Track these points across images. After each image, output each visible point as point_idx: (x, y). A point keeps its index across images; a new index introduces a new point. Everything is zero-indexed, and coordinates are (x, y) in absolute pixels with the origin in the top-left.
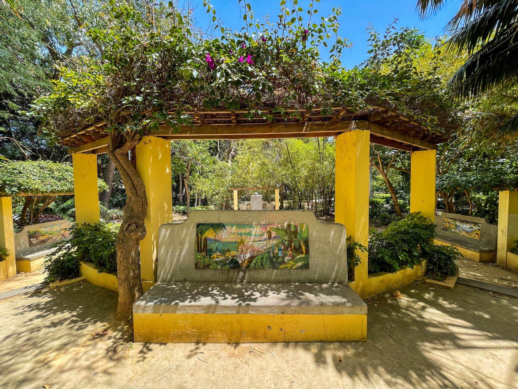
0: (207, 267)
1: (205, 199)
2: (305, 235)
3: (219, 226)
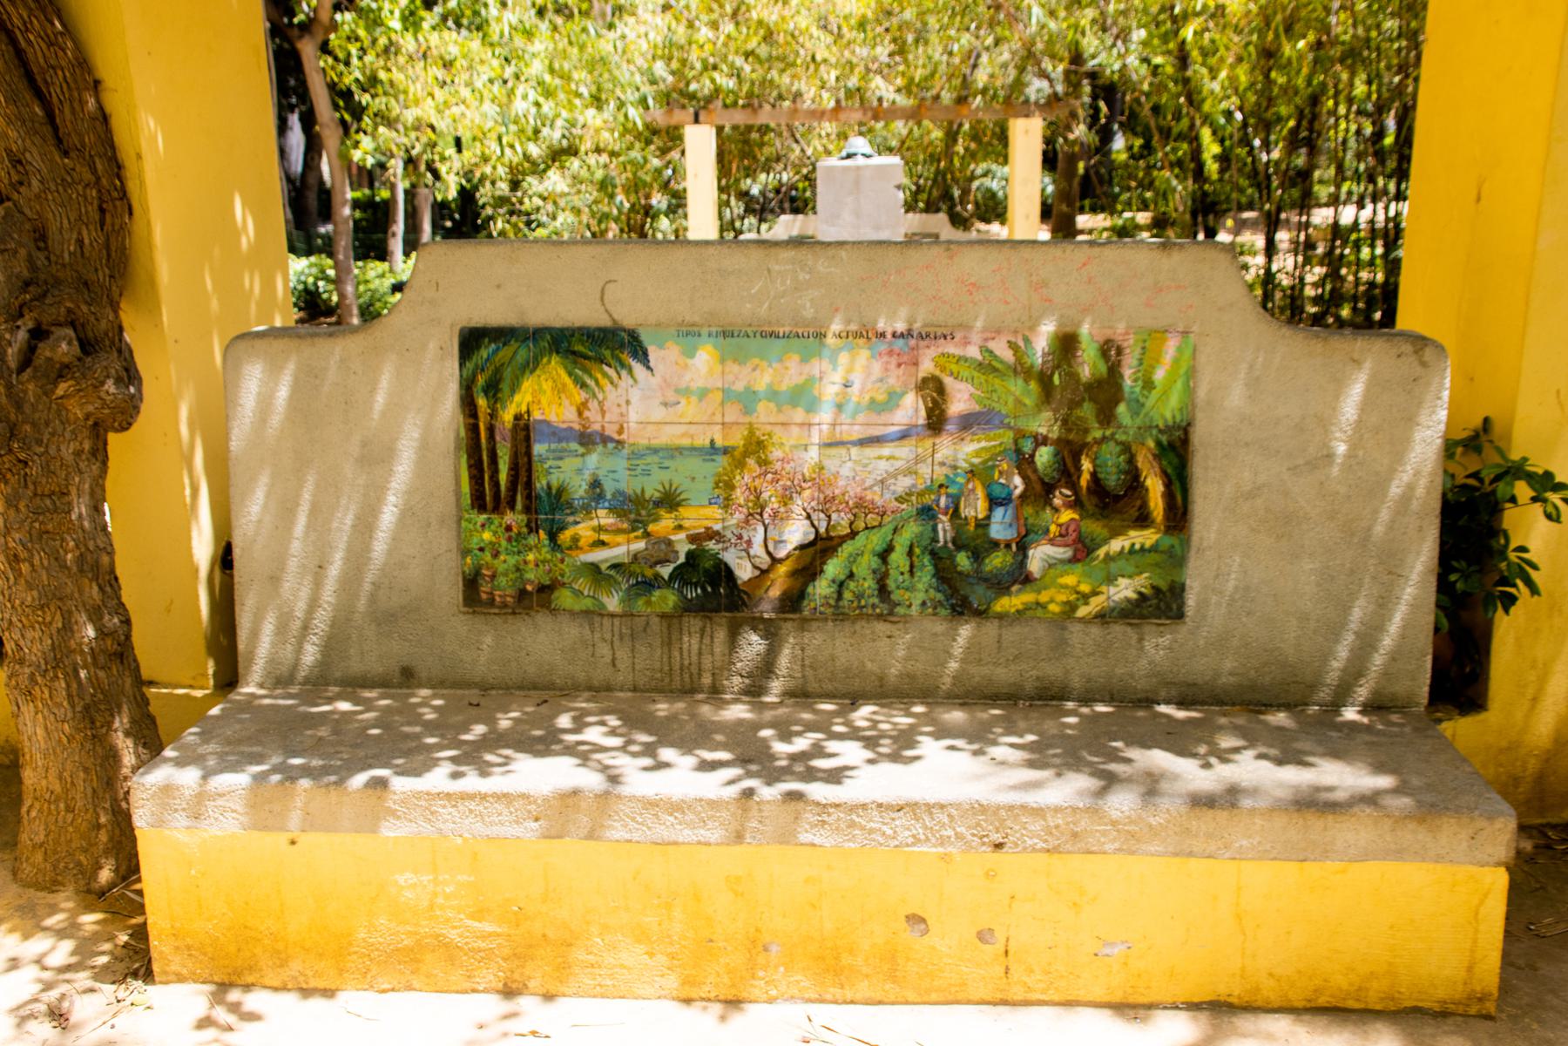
0: (536, 598)
1: (467, 196)
2: (1166, 409)
3: (604, 347)
